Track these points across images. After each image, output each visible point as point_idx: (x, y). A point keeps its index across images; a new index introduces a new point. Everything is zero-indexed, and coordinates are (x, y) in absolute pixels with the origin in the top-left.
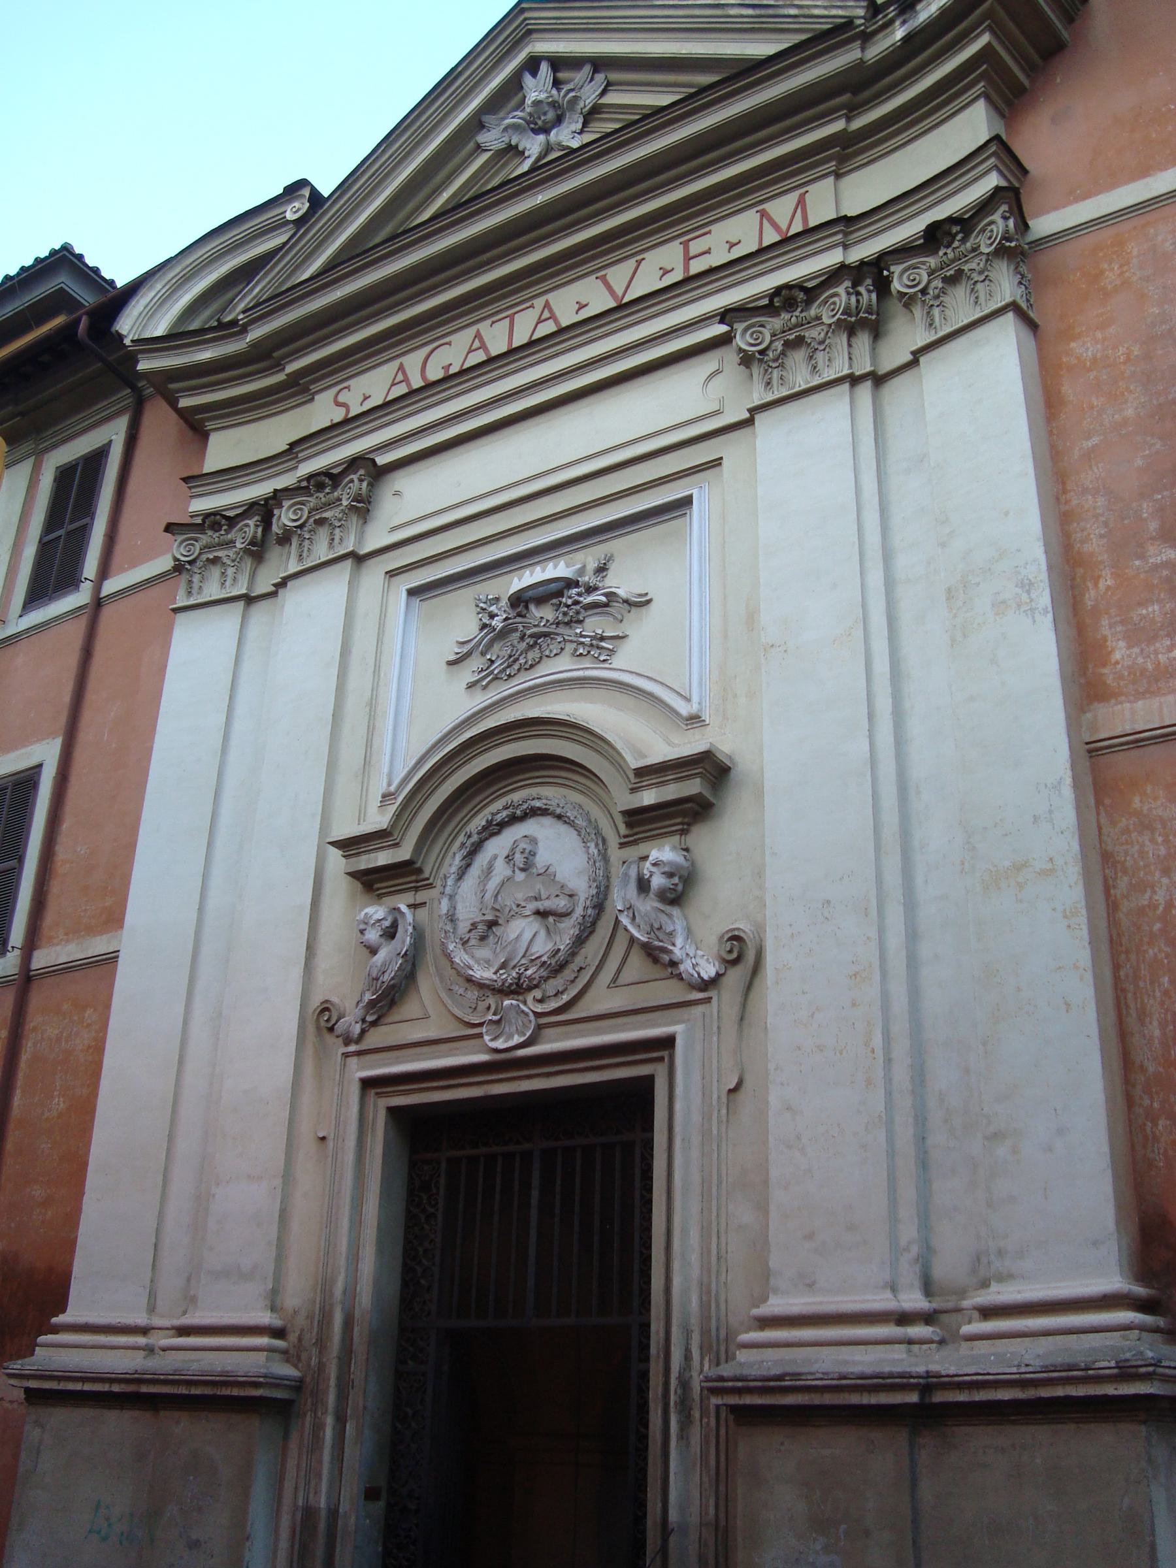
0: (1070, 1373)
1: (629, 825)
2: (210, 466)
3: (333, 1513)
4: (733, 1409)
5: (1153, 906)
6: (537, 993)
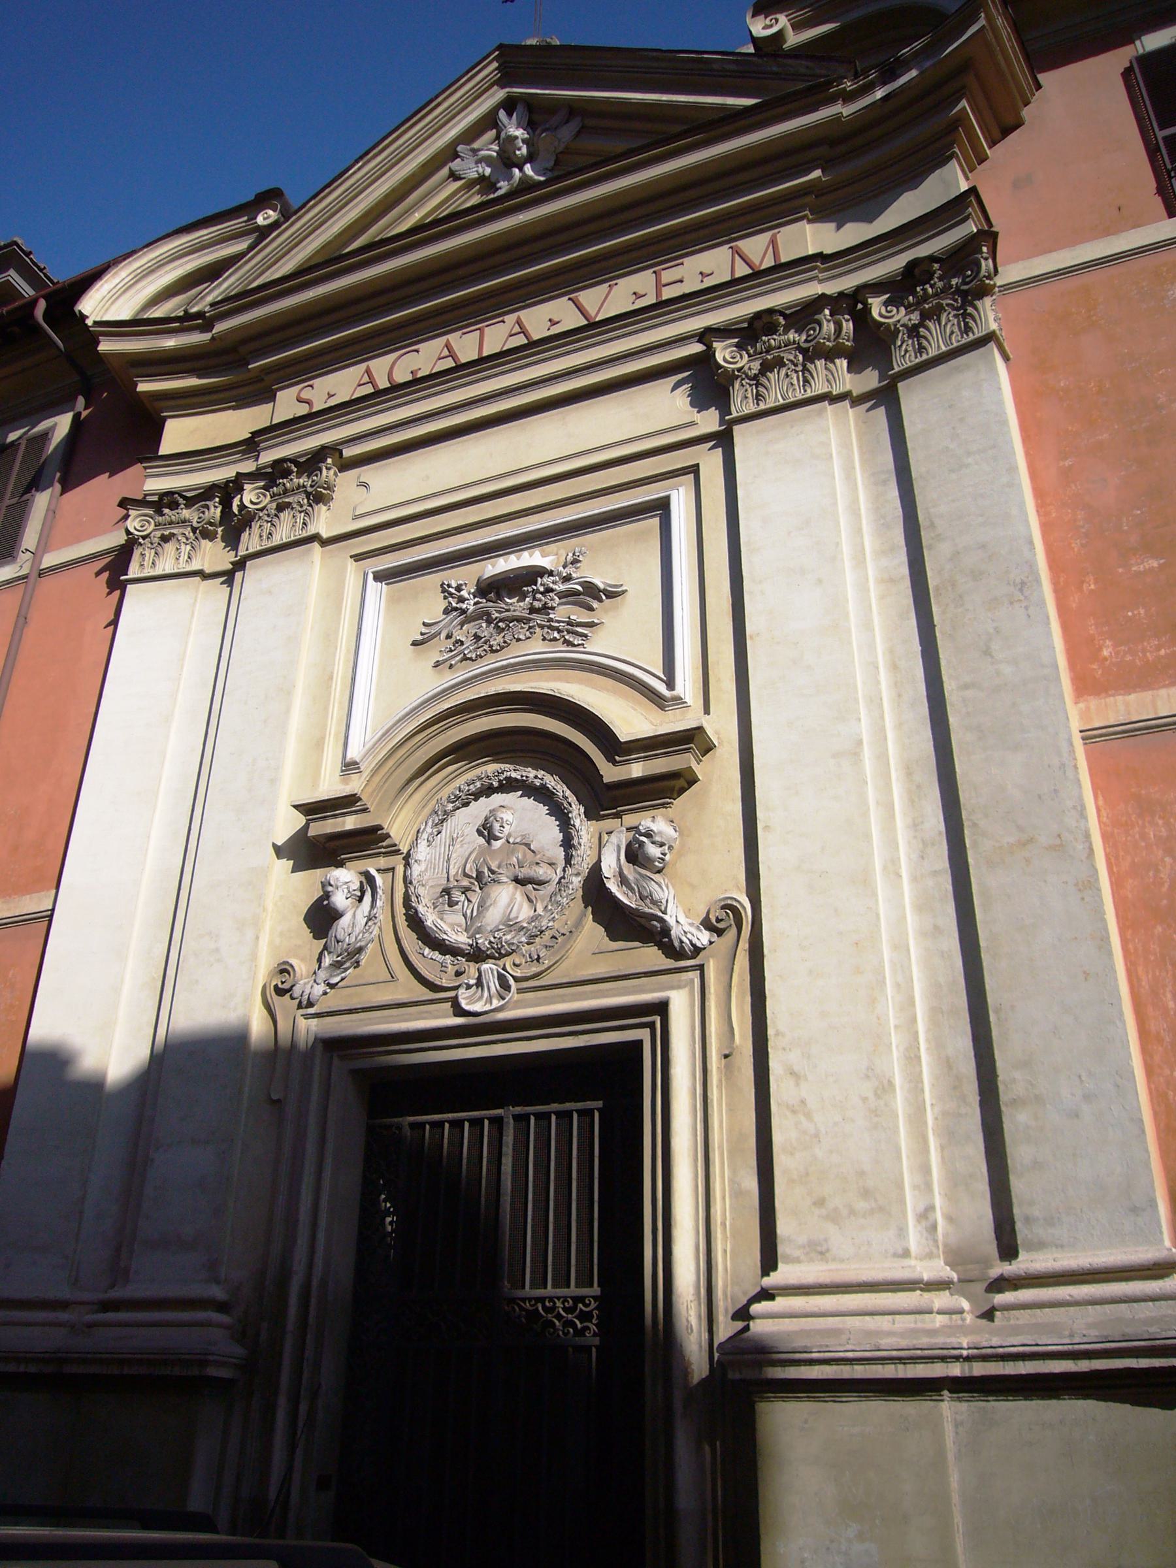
2: (163, 451)
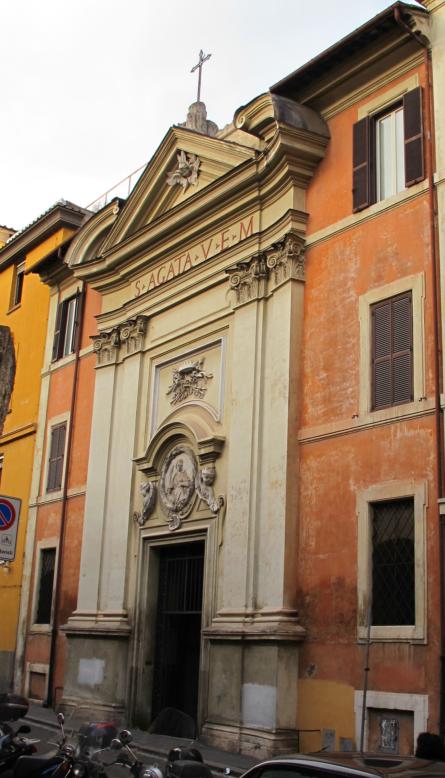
0: (264, 633)
1: (202, 459)
3: (137, 668)
4: (210, 640)
5: (308, 495)
6: (181, 512)
